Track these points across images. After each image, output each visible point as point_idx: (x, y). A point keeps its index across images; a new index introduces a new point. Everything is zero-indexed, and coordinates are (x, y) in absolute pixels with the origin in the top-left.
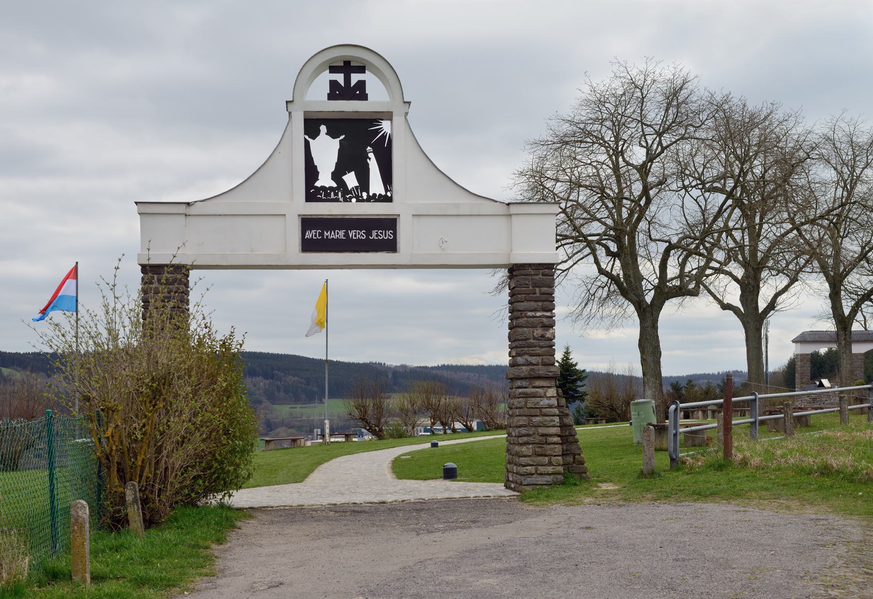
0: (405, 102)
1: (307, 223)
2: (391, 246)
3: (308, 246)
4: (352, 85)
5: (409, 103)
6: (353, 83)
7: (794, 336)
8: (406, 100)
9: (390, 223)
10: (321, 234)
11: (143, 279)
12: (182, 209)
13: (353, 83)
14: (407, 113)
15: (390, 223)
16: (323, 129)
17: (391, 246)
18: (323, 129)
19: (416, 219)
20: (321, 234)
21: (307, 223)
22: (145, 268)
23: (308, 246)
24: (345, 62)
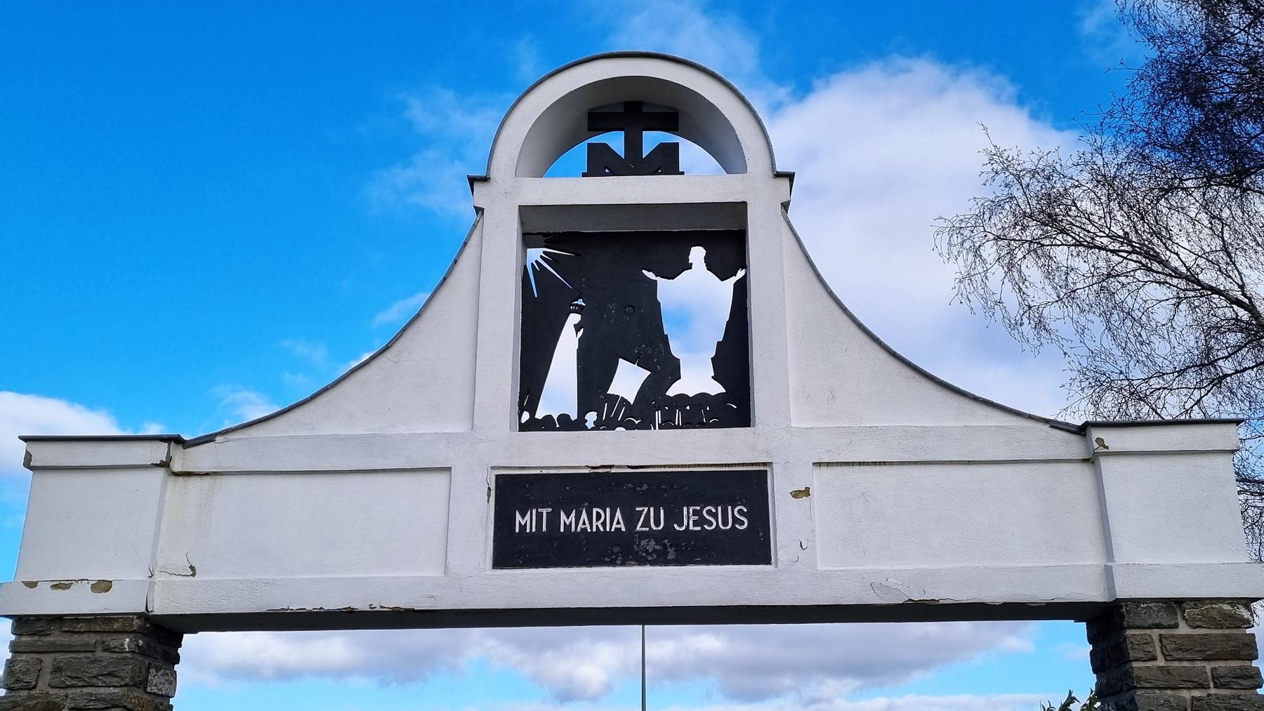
0: (778, 175)
1: (513, 491)
2: (753, 546)
3: (511, 550)
4: (672, 392)
5: (790, 177)
6: (647, 150)
7: (472, 174)
8: (779, 169)
9: (748, 486)
10: (554, 520)
11: (10, 663)
12: (158, 452)
13: (647, 150)
14: (785, 206)
15: (748, 486)
16: (697, 254)
17: (753, 546)
18: (697, 254)
19: (817, 469)
20: (554, 520)
21: (513, 491)
22: (22, 623)
23: (511, 550)
24: (628, 105)
